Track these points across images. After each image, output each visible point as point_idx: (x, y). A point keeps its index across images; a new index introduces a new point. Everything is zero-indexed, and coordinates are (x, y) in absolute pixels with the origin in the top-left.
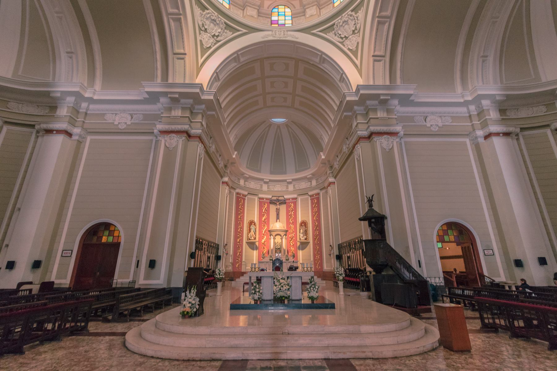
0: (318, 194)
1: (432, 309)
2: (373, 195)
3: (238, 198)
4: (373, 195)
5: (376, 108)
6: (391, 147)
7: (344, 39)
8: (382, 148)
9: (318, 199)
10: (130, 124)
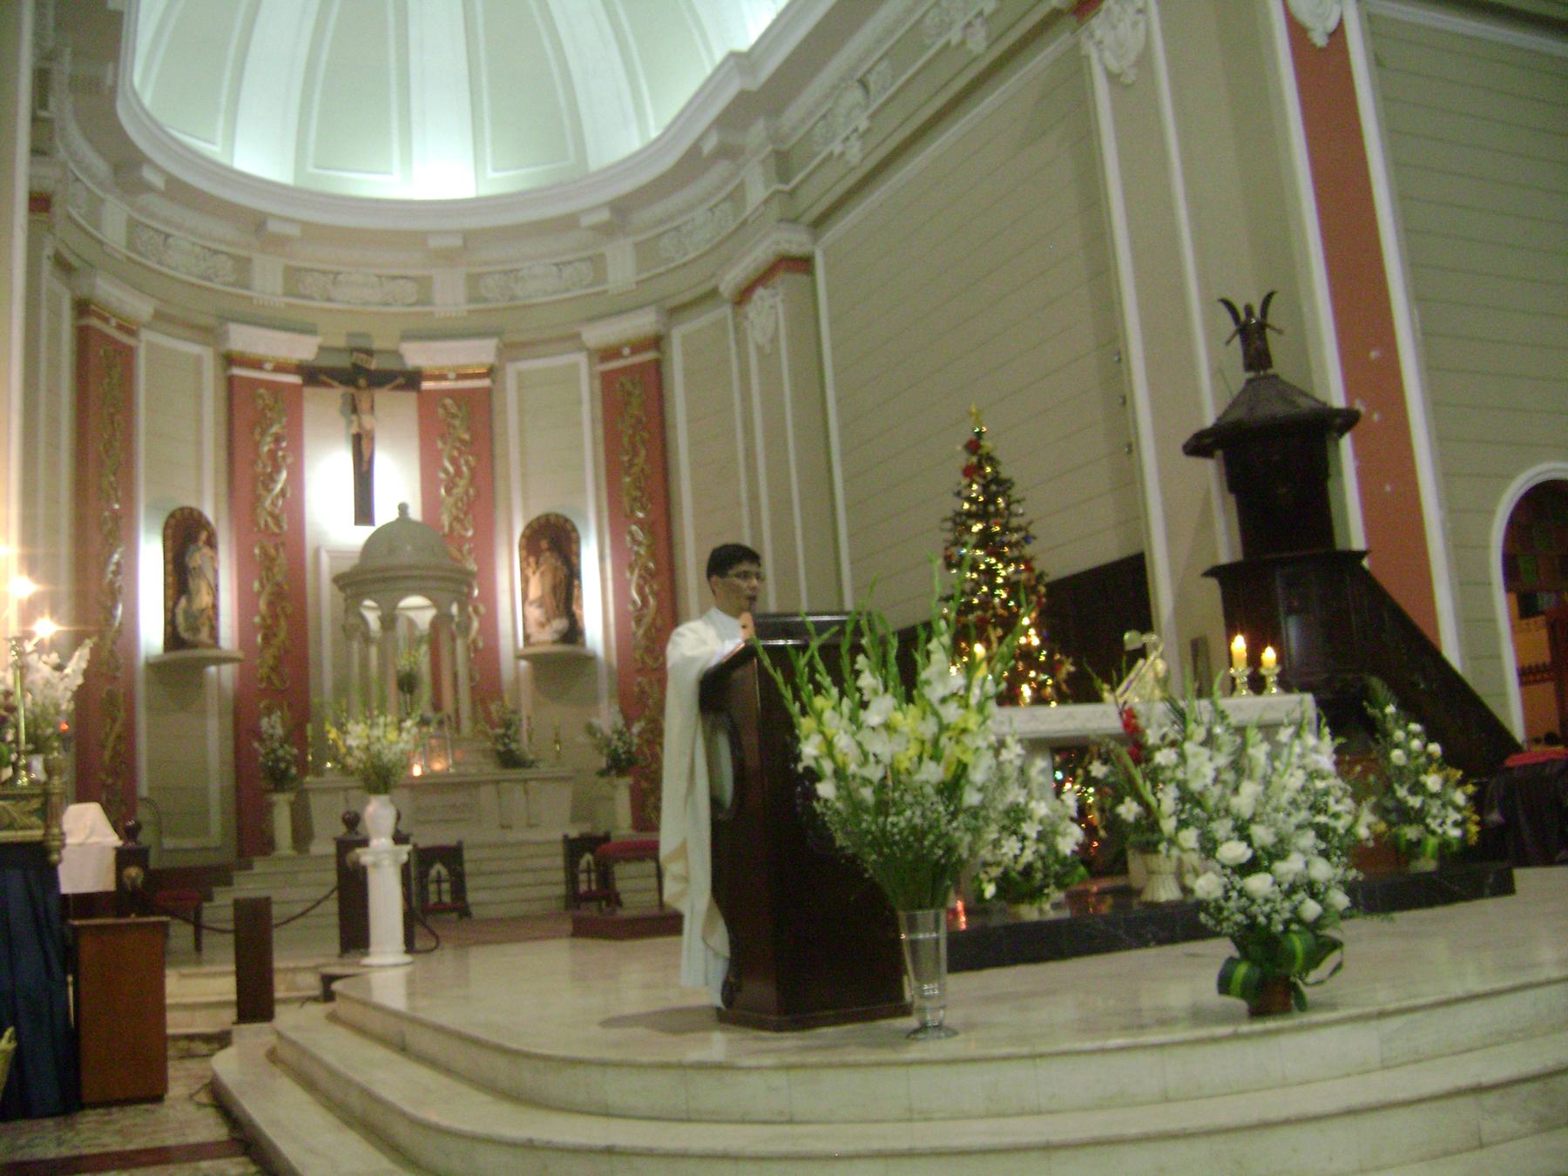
0: (657, 342)
2: (1269, 297)
3: (83, 336)
4: (1269, 297)
6: (1331, 24)
9: (654, 375)
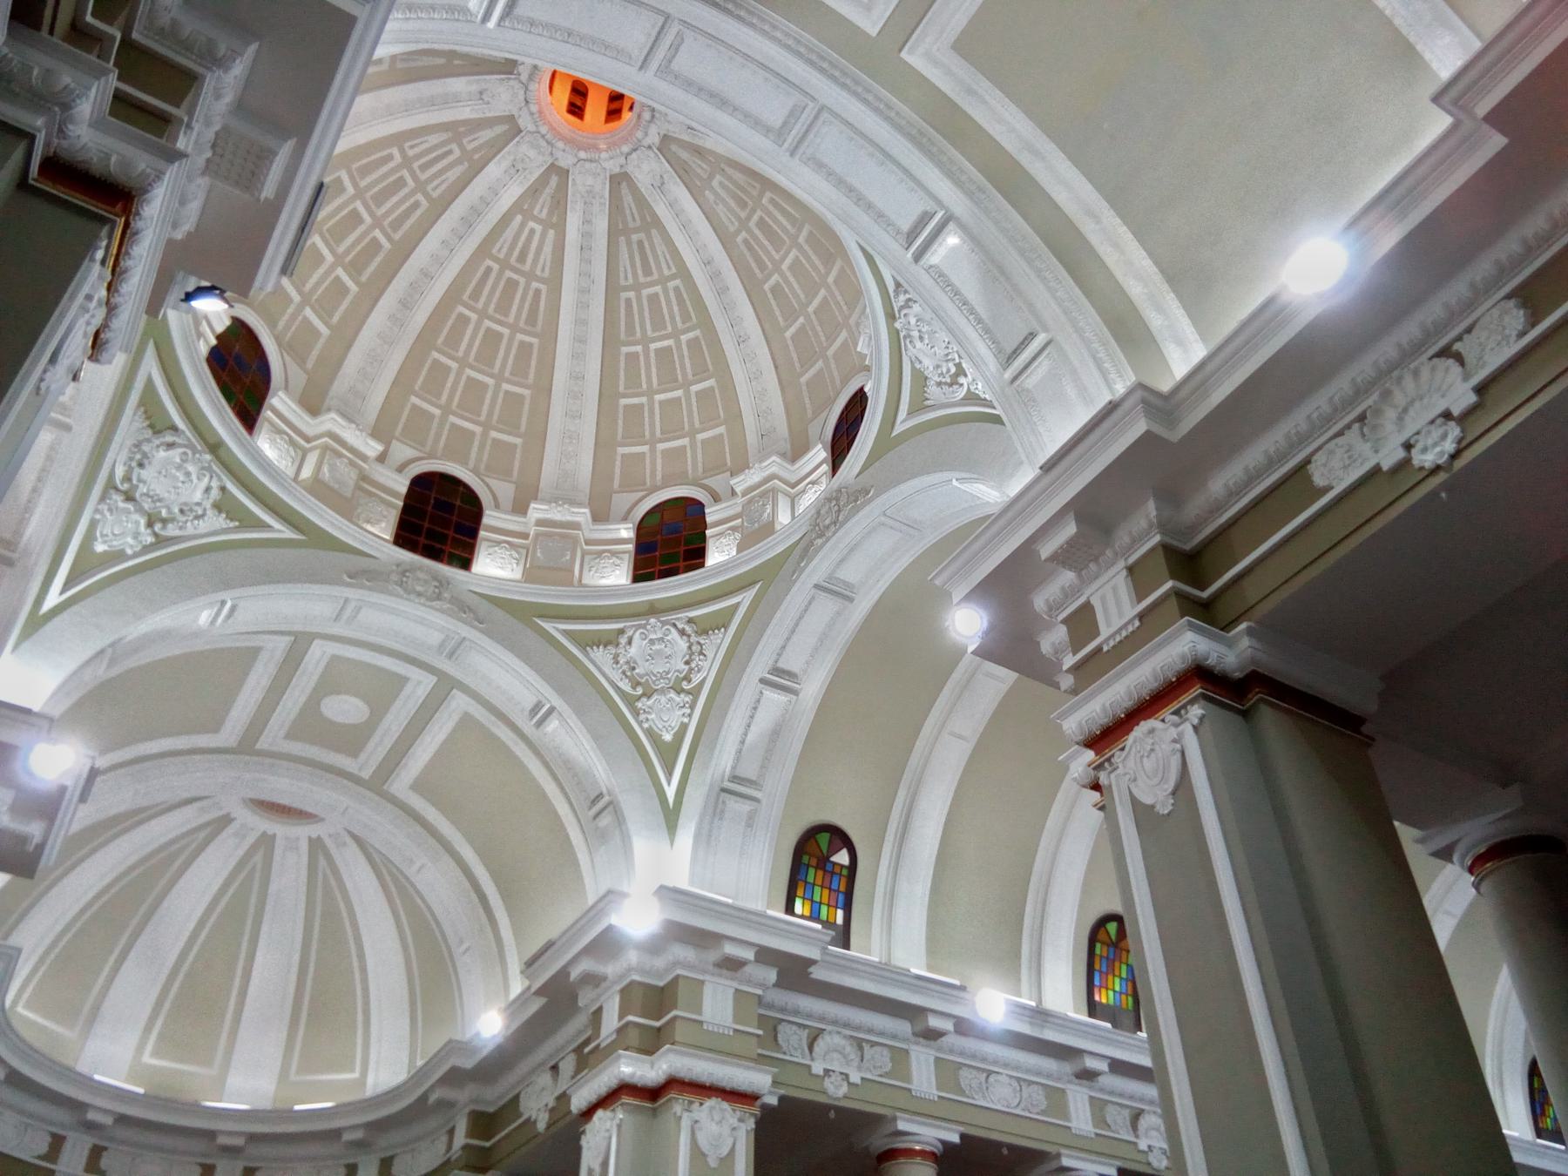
1: (383, 1156)
5: (700, 977)
6: (725, 1151)
7: (640, 691)
8: (697, 1154)
10: (1472, 398)
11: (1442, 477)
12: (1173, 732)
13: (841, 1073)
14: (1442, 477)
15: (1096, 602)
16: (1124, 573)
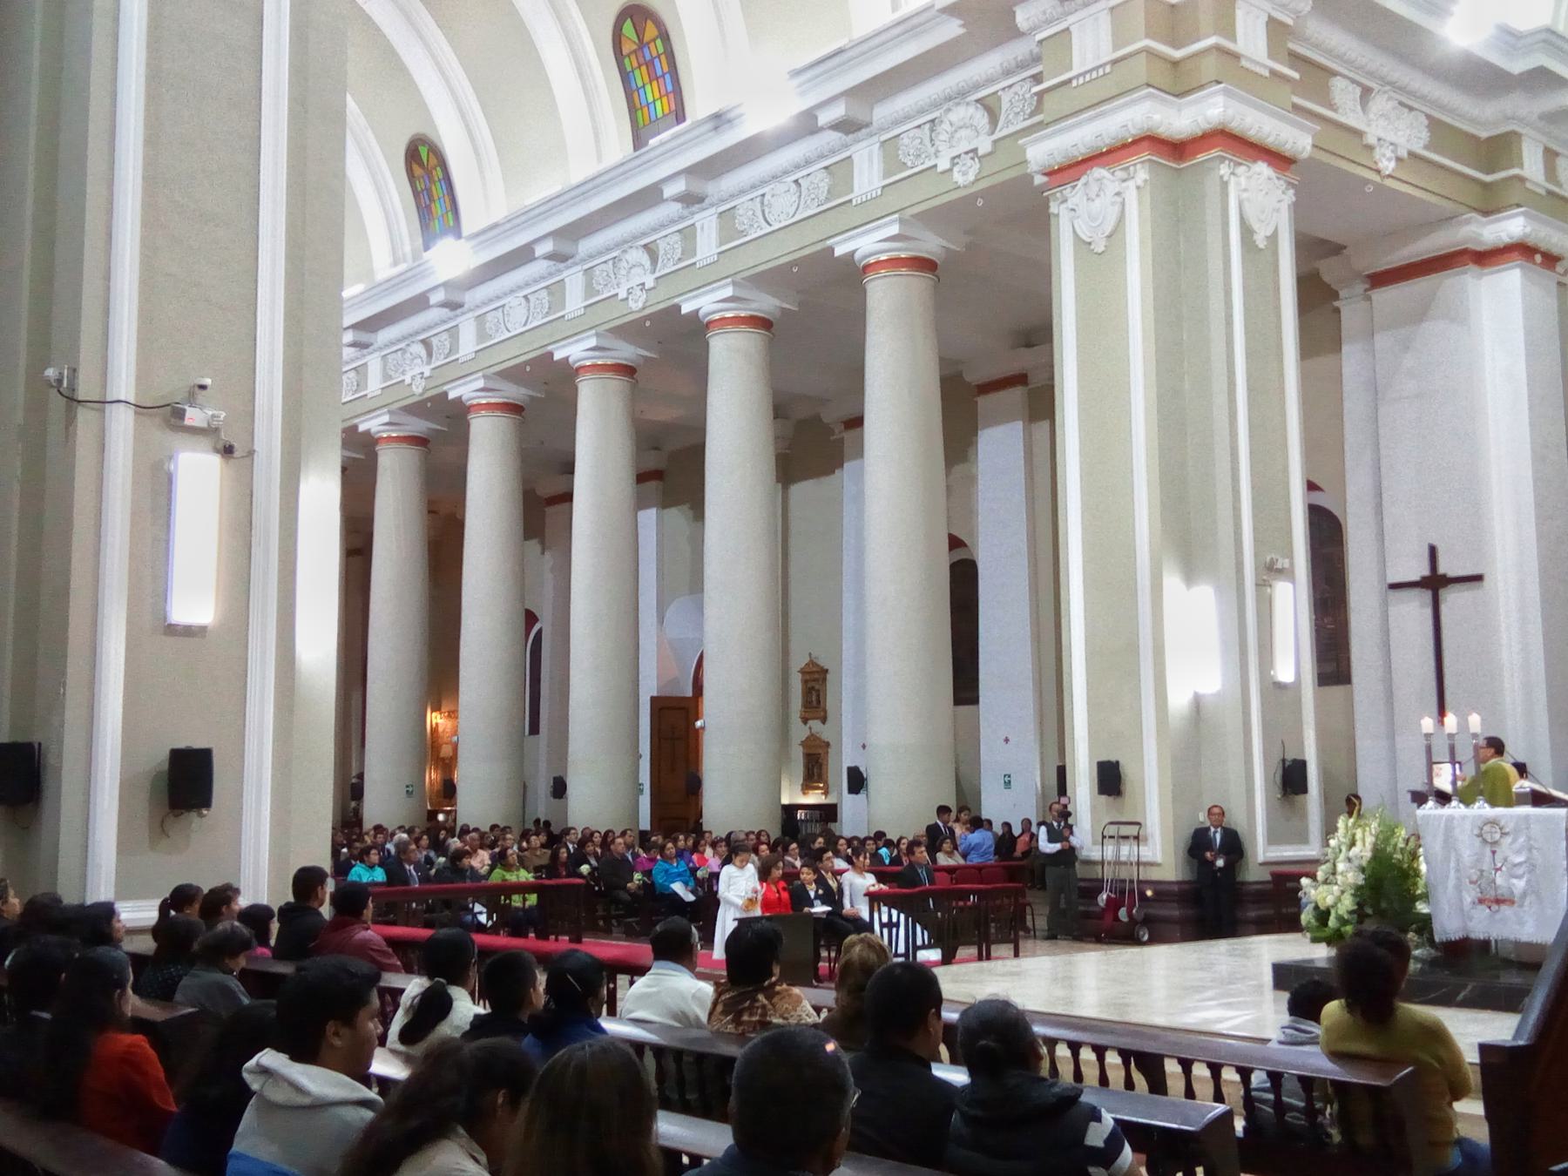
11: (1376, 178)
12: (1116, 187)
13: (1392, 144)
14: (1376, 178)
15: (698, 225)
16: (878, 145)
